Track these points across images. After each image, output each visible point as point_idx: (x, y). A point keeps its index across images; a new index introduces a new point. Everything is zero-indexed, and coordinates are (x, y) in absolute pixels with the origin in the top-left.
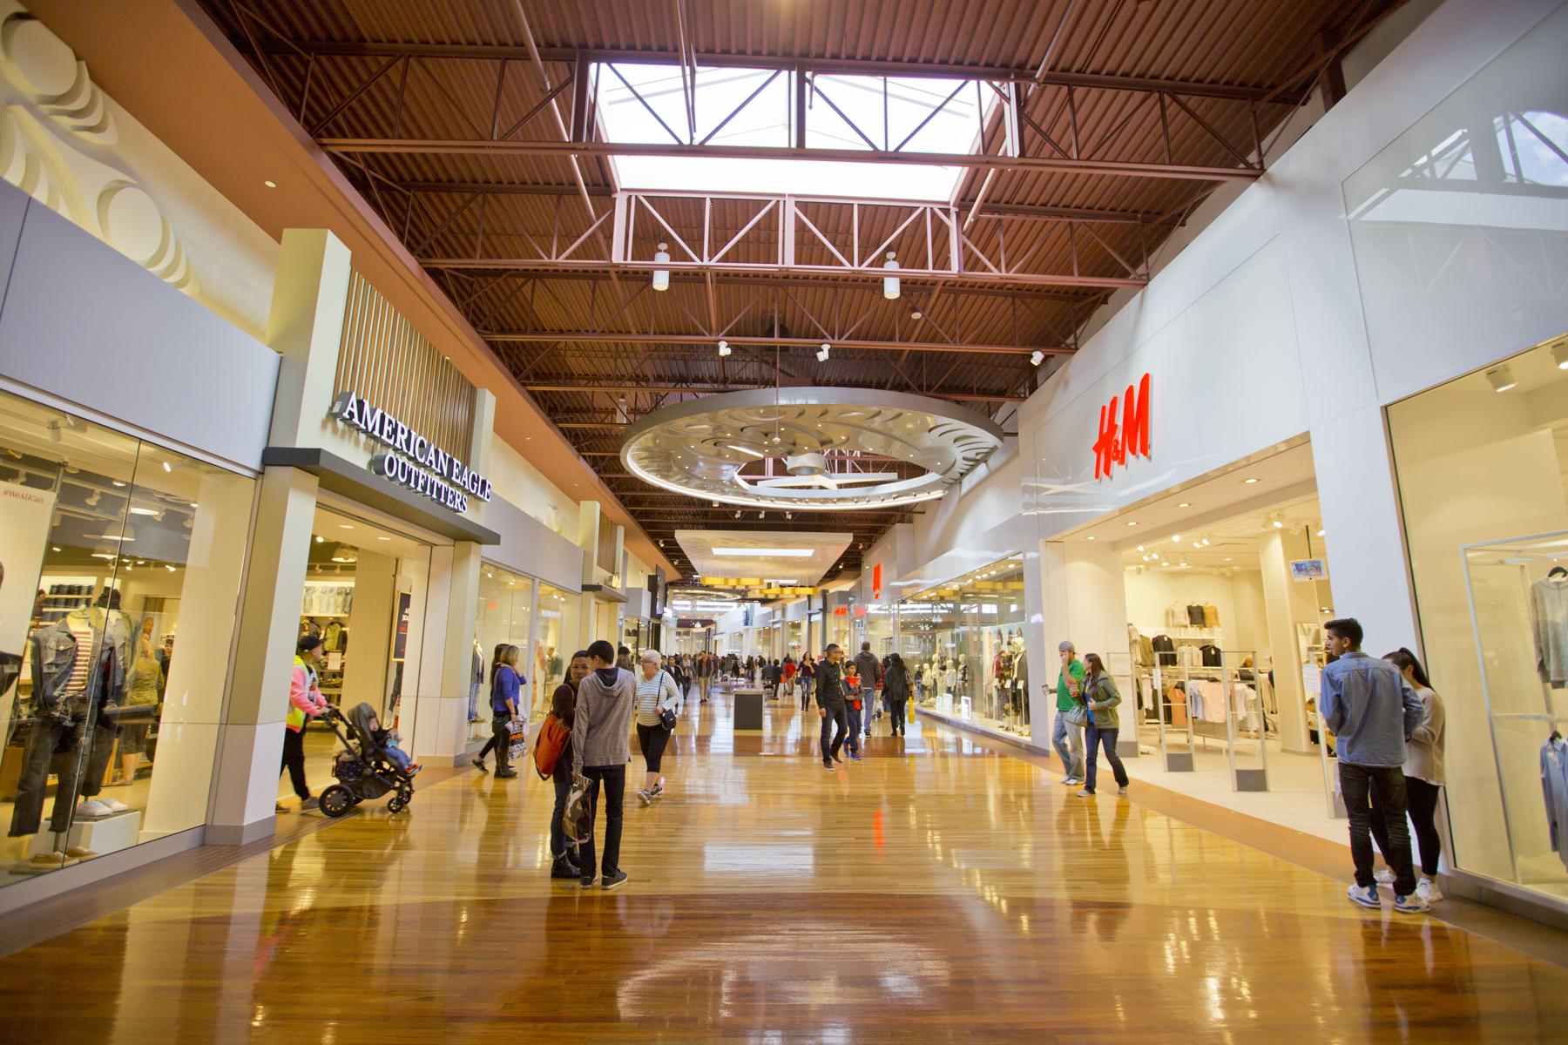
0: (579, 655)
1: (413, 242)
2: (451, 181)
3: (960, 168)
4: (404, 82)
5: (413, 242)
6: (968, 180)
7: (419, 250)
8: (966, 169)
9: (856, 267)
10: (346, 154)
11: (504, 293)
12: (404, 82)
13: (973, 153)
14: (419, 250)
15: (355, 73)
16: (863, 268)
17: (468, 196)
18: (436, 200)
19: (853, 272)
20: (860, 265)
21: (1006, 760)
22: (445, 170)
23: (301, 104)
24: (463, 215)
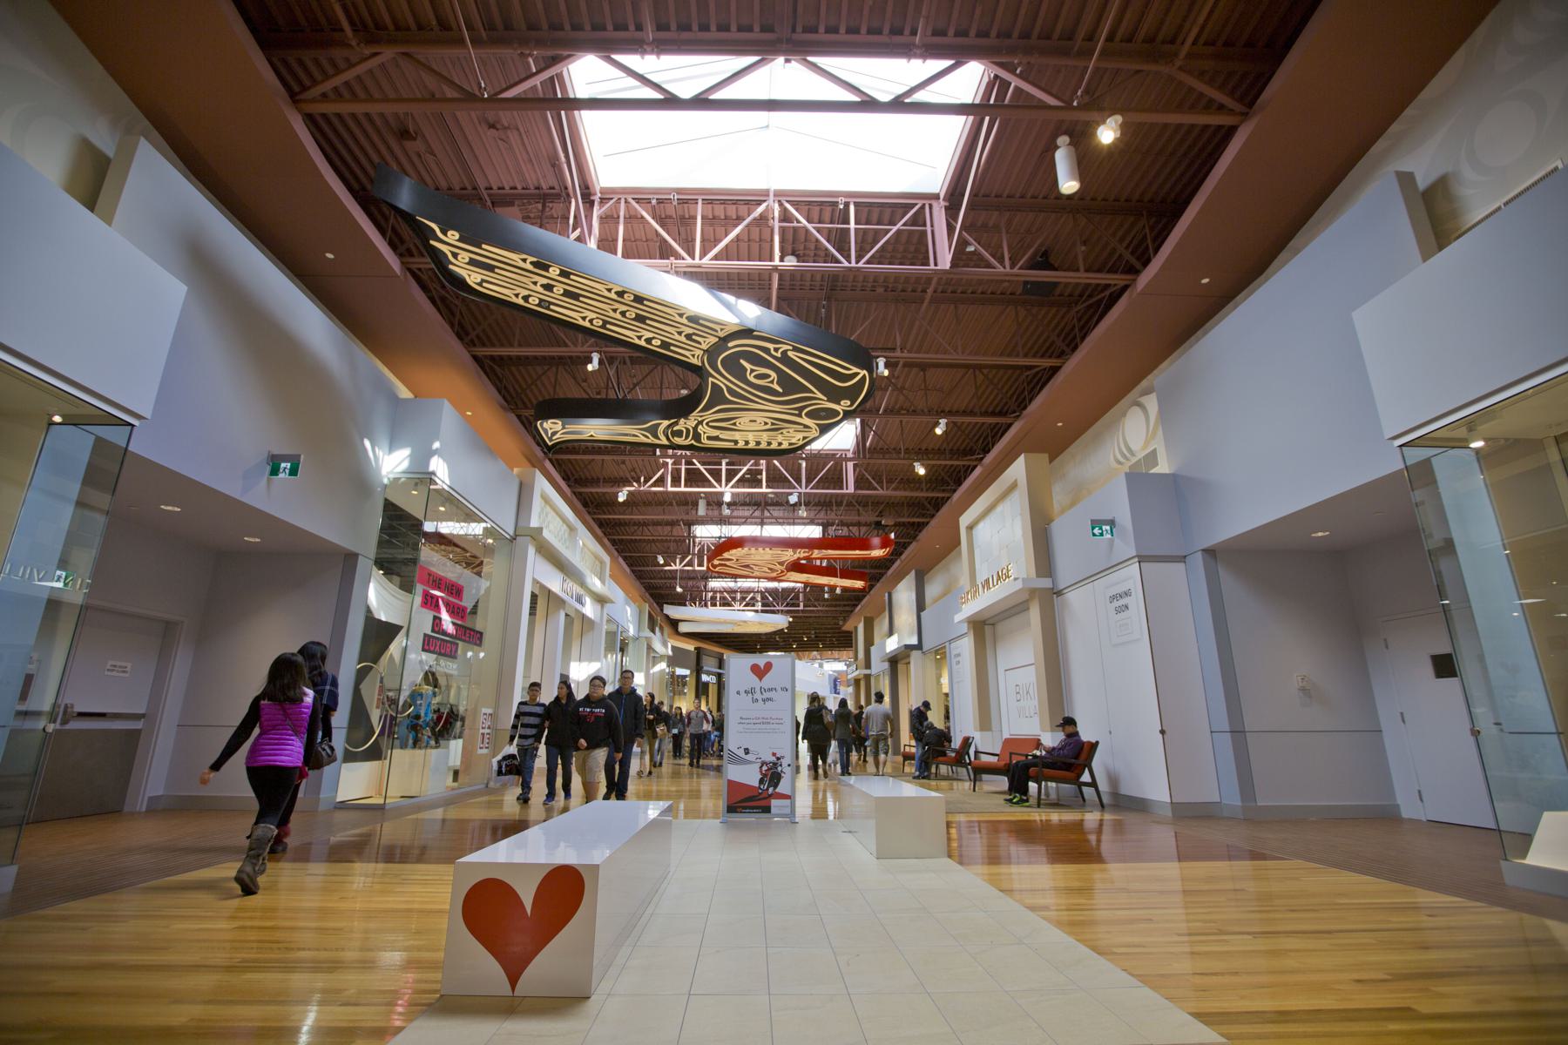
0: (544, 804)
1: (396, 240)
2: (593, 479)
3: (965, 117)
4: (556, 379)
5: (396, 240)
6: (969, 143)
7: (402, 249)
8: (971, 118)
9: (853, 264)
10: (420, 269)
11: (520, 386)
12: (556, 379)
13: (977, 101)
14: (402, 249)
15: (523, 377)
16: (860, 265)
17: (546, 368)
18: (516, 373)
19: (850, 269)
20: (857, 262)
21: (1003, 869)
22: (444, 175)
23: (388, 227)
24: (536, 385)
